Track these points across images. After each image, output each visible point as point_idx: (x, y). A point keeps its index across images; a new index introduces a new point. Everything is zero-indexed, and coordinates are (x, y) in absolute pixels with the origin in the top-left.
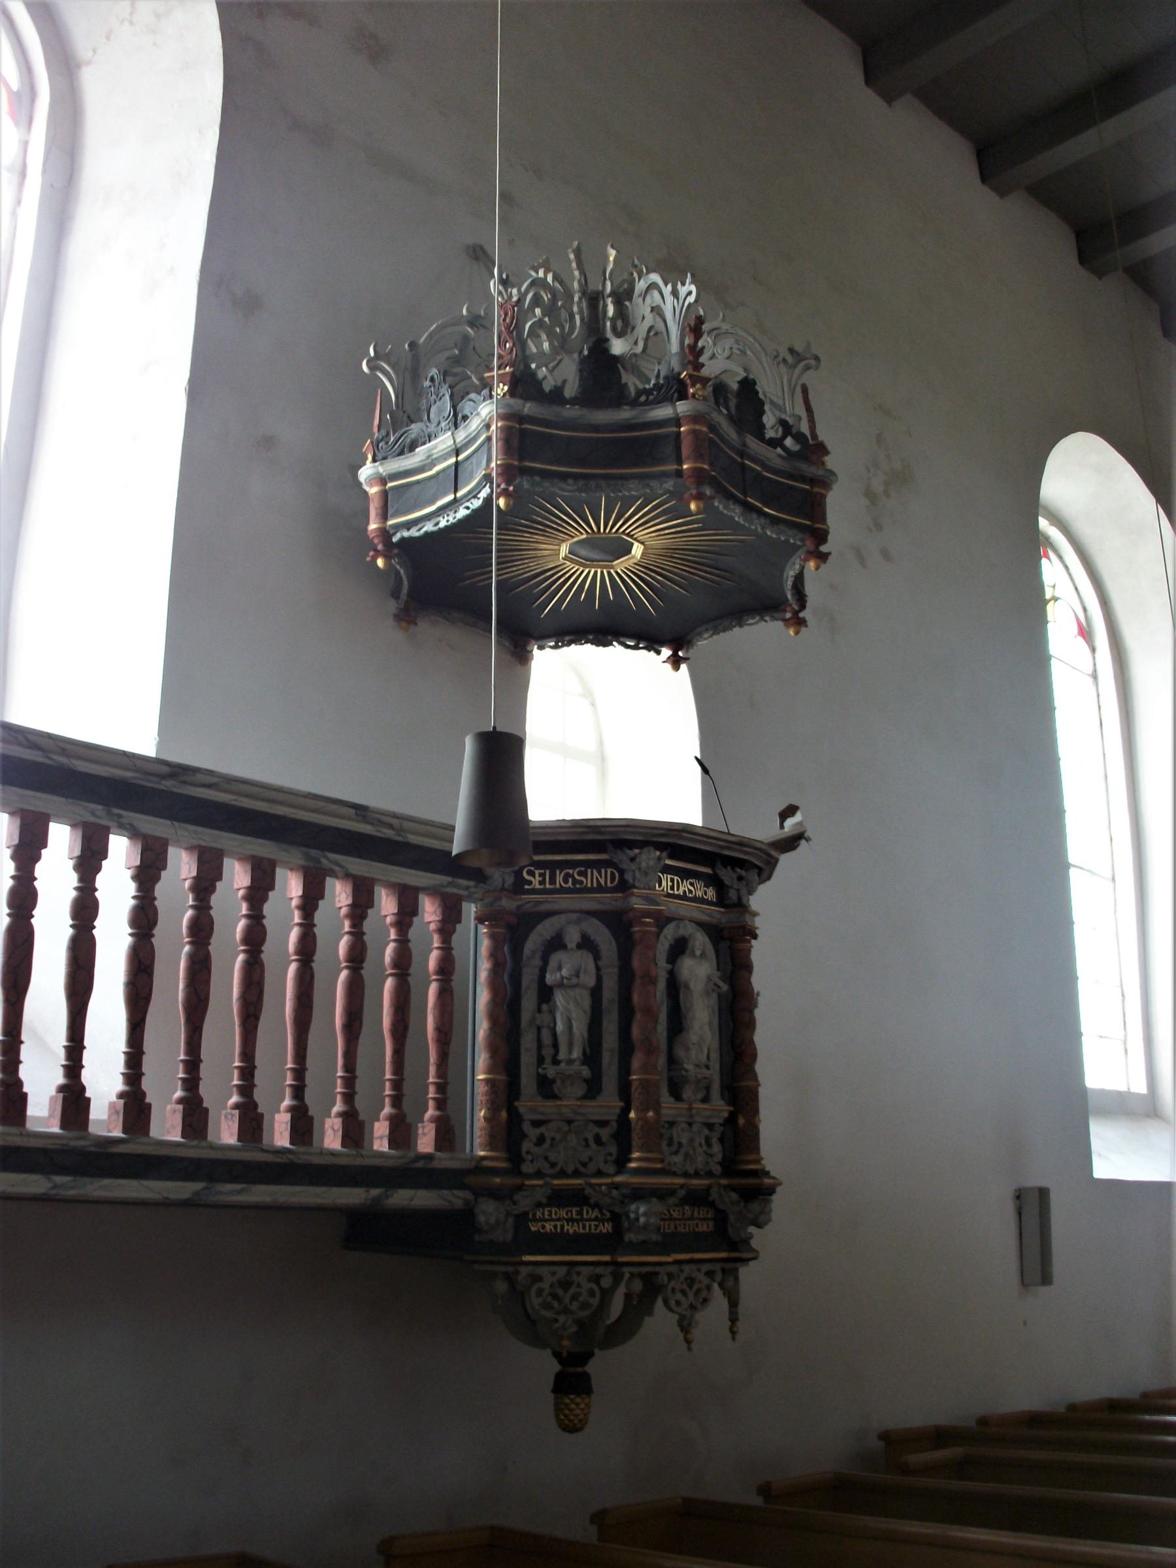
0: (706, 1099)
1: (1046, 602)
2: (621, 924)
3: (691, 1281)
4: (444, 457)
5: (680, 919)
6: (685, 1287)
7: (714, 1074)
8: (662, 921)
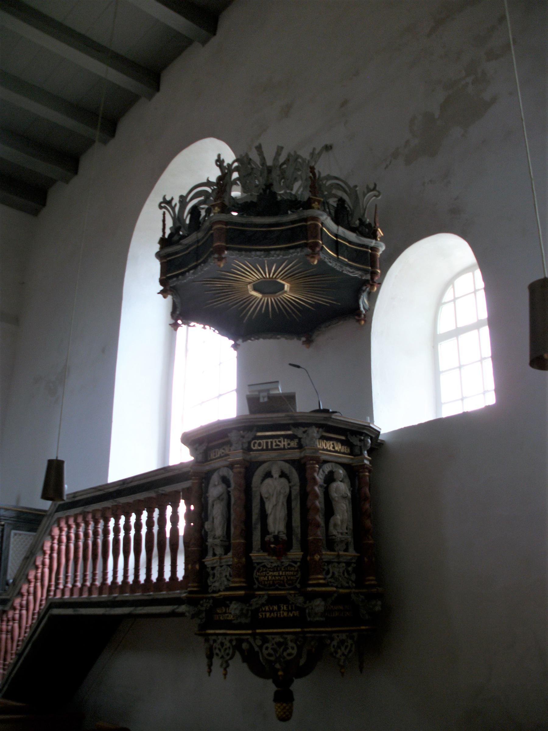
0: (346, 550)
2: (301, 466)
3: (222, 644)
6: (220, 647)
7: (350, 538)
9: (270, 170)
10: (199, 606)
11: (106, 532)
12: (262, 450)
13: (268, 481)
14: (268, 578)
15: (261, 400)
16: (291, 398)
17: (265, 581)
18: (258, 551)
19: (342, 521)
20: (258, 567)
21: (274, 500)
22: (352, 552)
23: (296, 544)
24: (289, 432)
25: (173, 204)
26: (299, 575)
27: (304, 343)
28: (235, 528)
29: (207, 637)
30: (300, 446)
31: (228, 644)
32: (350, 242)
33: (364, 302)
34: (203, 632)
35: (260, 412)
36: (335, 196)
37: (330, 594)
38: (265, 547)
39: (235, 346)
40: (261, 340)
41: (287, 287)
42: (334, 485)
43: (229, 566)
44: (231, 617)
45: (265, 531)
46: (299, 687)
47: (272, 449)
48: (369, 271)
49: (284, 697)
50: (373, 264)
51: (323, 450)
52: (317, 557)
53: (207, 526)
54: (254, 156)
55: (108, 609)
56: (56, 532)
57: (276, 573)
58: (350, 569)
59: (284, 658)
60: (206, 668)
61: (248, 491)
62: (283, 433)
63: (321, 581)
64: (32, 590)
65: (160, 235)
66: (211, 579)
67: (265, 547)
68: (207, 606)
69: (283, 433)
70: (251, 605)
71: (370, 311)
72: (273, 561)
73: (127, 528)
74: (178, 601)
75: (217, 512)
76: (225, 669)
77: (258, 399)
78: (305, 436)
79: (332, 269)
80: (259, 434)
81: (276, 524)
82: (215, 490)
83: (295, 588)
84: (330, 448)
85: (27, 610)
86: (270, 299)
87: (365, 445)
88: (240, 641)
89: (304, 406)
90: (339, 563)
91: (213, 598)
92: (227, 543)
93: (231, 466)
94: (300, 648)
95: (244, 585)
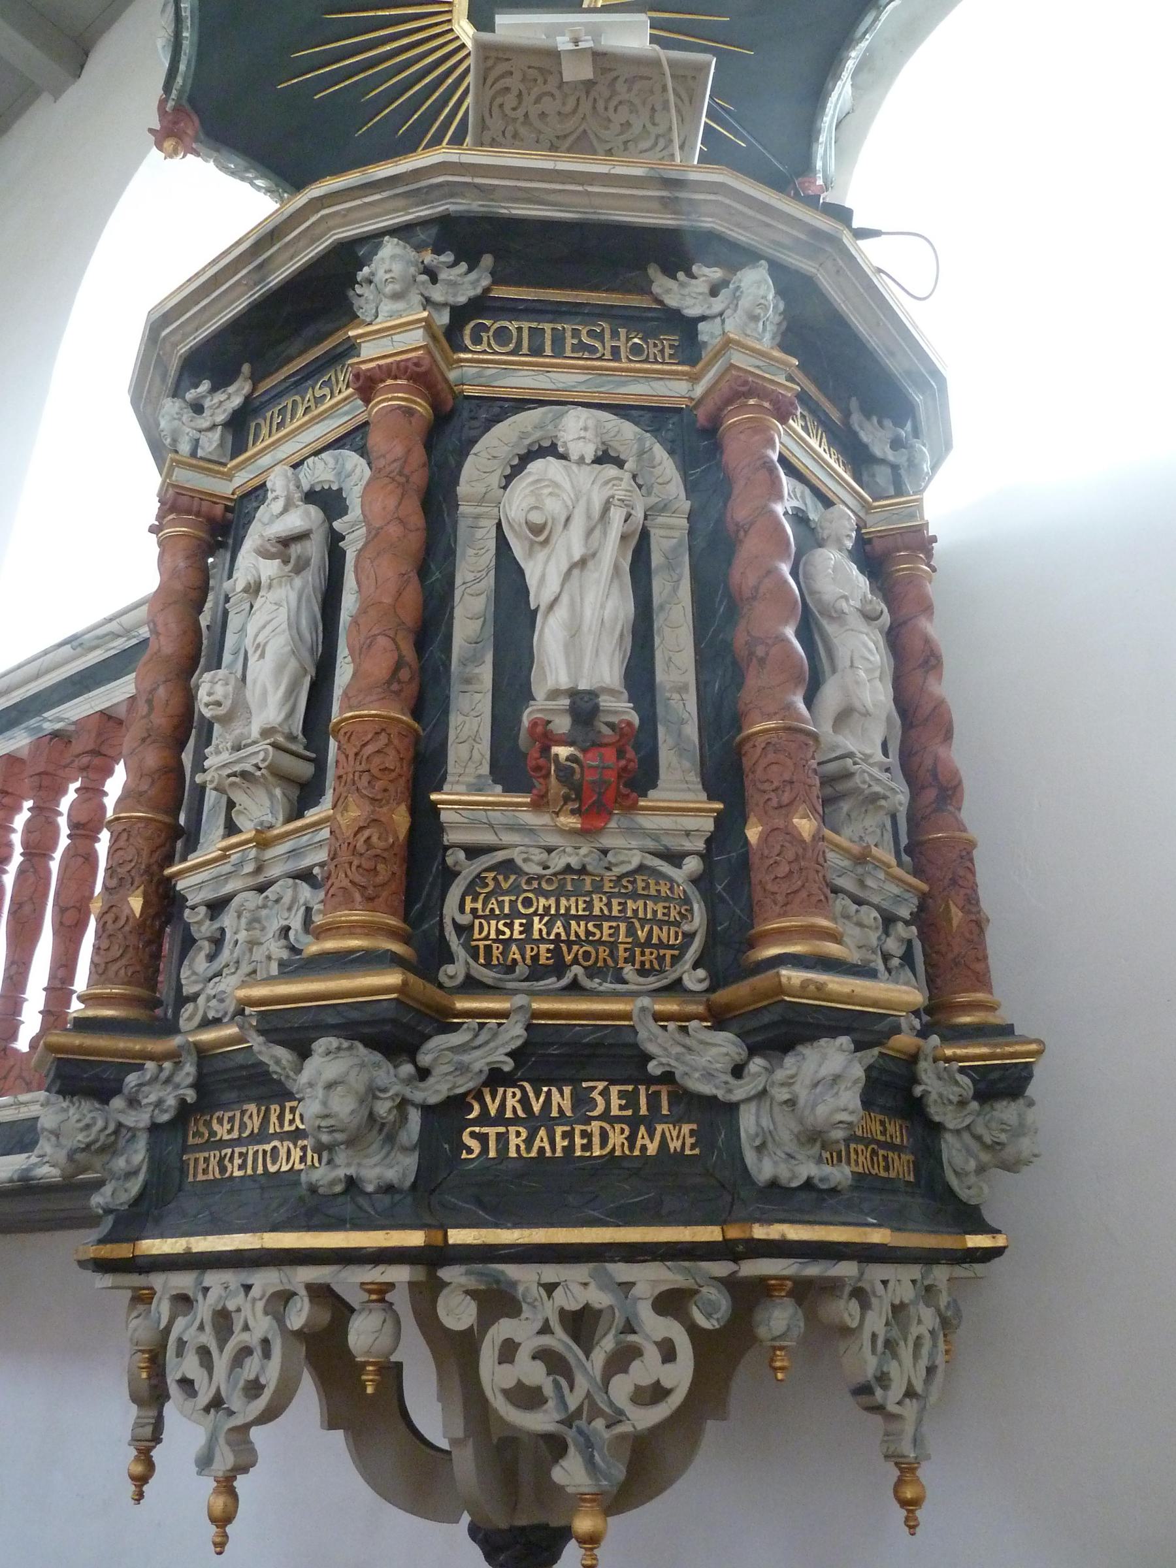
3: (223, 1321)
6: (208, 1339)
10: (117, 1103)
14: (527, 928)
17: (507, 943)
20: (470, 869)
21: (572, 543)
26: (698, 920)
28: (359, 654)
31: (257, 1324)
34: (122, 1251)
38: (513, 766)
43: (305, 876)
57: (577, 906)
59: (617, 1417)
66: (199, 962)
67: (513, 766)
68: (159, 1103)
70: (423, 1074)
72: (552, 840)
76: (227, 1486)
83: (675, 988)
92: (306, 770)
95: (397, 947)
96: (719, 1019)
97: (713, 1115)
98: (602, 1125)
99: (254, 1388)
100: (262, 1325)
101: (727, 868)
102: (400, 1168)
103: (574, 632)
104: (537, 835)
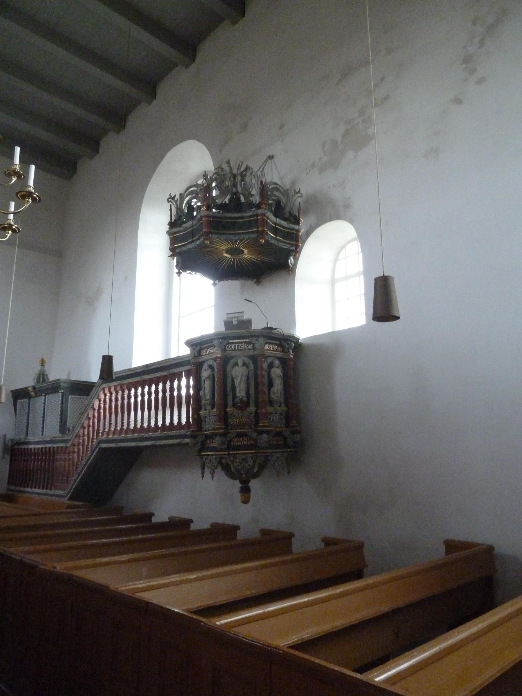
0: (280, 406)
1: (215, 281)
3: (211, 460)
4: (190, 228)
5: (208, 360)
7: (282, 400)
8: (266, 357)
9: (235, 176)
11: (129, 397)
12: (232, 350)
13: (236, 368)
15: (234, 323)
16: (249, 322)
18: (231, 408)
19: (278, 390)
22: (283, 408)
23: (252, 404)
24: (248, 340)
25: (176, 199)
27: (255, 283)
29: (201, 456)
30: (254, 348)
32: (284, 227)
33: (291, 261)
35: (231, 329)
36: (275, 195)
37: (272, 431)
38: (234, 405)
39: (214, 284)
40: (230, 281)
41: (246, 251)
42: (273, 370)
44: (215, 445)
45: (234, 396)
46: (253, 484)
47: (238, 350)
48: (294, 242)
49: (245, 490)
50: (297, 241)
51: (267, 350)
52: (264, 410)
53: (201, 393)
54: (225, 167)
55: (138, 443)
56: (102, 396)
58: (282, 417)
60: (201, 475)
61: (224, 373)
62: (244, 340)
63: (266, 424)
64: (86, 433)
65: (168, 220)
67: (234, 405)
69: (244, 340)
71: (295, 265)
73: (150, 394)
74: (184, 436)
75: (207, 385)
77: (232, 322)
78: (256, 342)
79: (272, 244)
80: (231, 341)
81: (241, 393)
82: (205, 373)
83: (251, 428)
84: (270, 349)
85: (83, 446)
86: (235, 258)
87: (291, 347)
88: (221, 458)
89: (257, 325)
90: (276, 414)
91: (205, 434)
93: (215, 359)
94: (254, 462)
96: (255, 431)
97: (256, 440)
98: (245, 441)
99: (214, 466)
100: (214, 461)
101: (257, 414)
102: (226, 446)
103: (240, 390)
104: (237, 412)
